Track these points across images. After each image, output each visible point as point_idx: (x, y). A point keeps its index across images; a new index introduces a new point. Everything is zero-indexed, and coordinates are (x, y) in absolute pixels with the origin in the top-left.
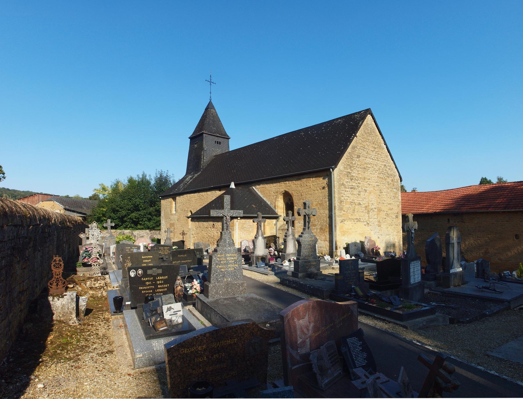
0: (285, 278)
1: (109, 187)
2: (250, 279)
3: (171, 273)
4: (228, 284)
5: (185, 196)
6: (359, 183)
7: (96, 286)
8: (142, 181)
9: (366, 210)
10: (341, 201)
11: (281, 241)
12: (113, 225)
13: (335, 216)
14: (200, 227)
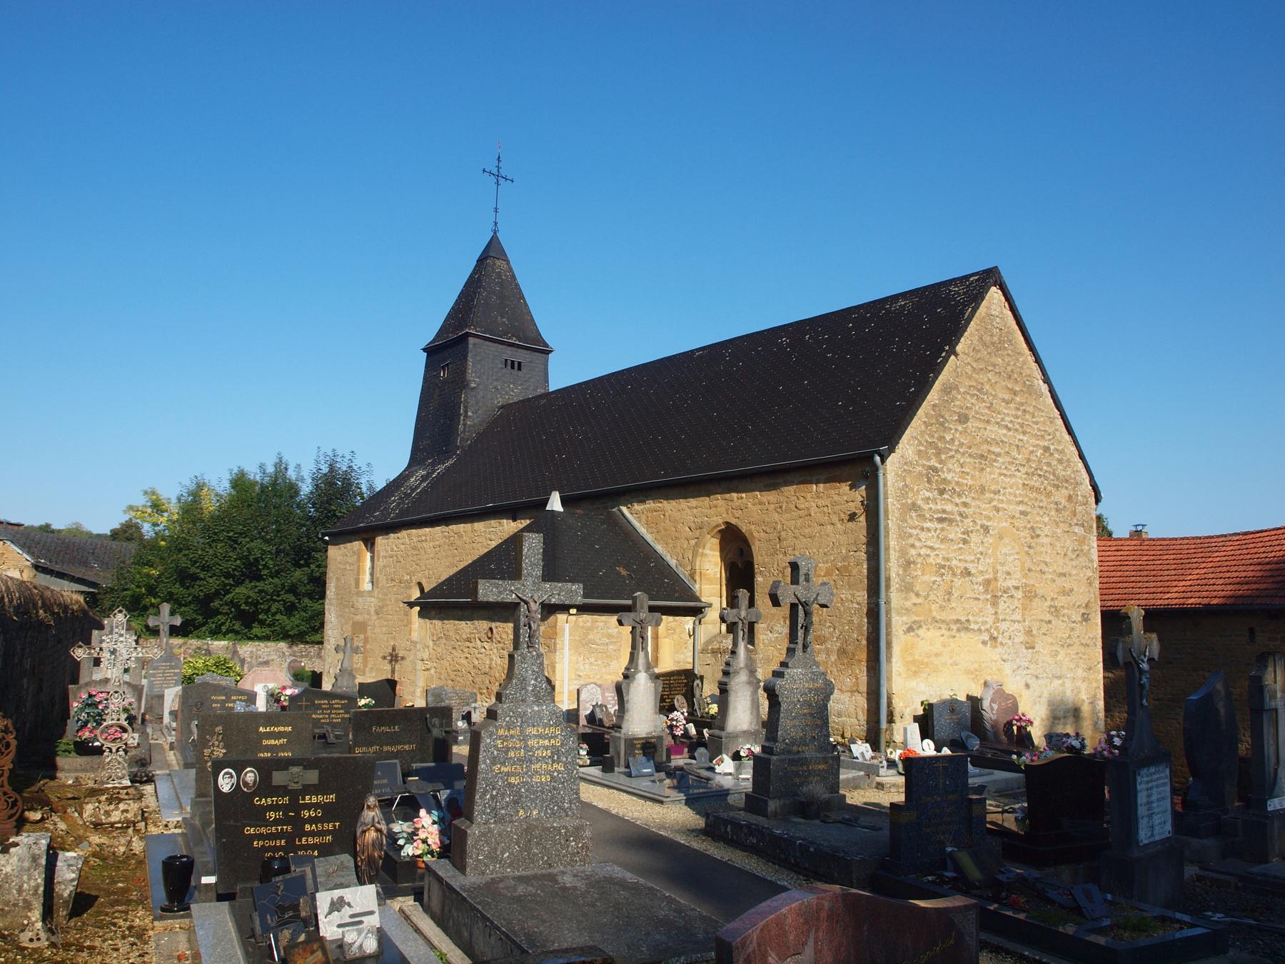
0: (723, 815)
1: (174, 500)
2: (605, 813)
3: (347, 784)
4: (529, 829)
5: (404, 533)
6: (965, 504)
7: (112, 819)
8: (274, 484)
9: (986, 591)
10: (909, 563)
11: (709, 689)
12: (178, 621)
13: (888, 612)
14: (447, 637)
